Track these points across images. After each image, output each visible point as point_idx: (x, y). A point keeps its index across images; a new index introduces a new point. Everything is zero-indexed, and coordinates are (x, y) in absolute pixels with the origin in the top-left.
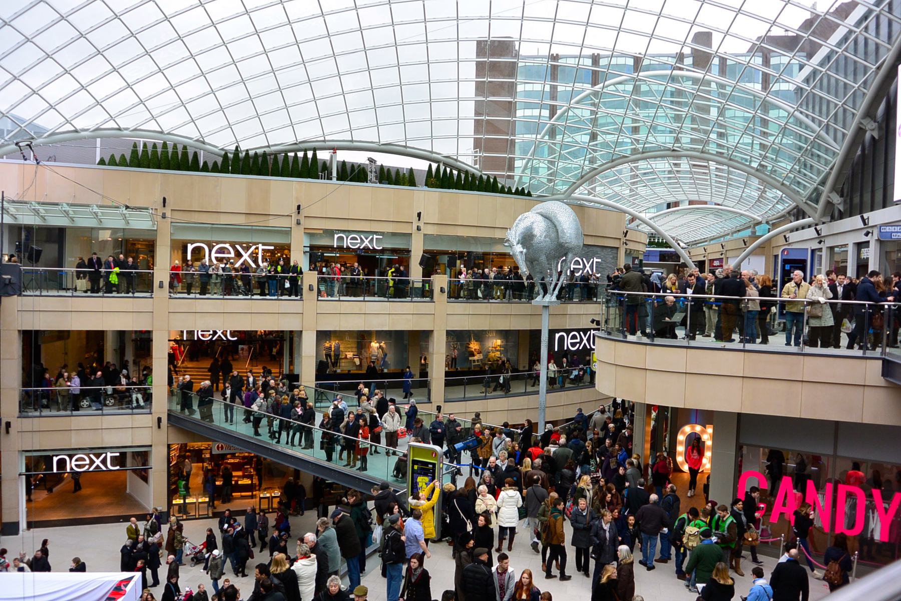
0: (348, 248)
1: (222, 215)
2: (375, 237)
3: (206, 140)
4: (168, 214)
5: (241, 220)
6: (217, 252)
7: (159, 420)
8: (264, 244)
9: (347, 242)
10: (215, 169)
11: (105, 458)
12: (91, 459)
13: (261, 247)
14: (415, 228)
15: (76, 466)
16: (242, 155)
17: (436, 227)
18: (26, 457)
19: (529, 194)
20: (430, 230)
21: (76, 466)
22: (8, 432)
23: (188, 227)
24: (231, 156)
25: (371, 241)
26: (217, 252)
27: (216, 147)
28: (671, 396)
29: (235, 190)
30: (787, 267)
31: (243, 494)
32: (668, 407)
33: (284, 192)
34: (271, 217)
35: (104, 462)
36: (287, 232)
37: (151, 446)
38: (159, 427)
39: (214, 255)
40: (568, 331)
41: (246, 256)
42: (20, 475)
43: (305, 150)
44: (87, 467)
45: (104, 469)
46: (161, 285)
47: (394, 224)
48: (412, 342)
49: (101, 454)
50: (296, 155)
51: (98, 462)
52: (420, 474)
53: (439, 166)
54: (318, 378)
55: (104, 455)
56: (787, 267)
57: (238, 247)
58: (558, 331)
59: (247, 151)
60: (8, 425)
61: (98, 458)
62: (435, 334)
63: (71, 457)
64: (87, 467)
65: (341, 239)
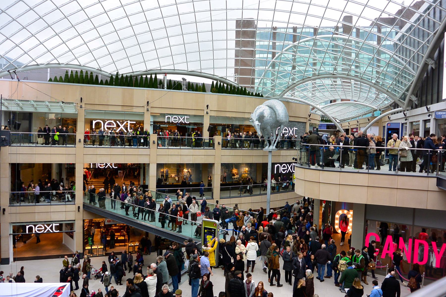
0: (172, 122)
1: (110, 106)
2: (186, 117)
3: (102, 69)
4: (83, 106)
5: (119, 109)
6: (107, 125)
7: (79, 207)
8: (131, 121)
9: (172, 120)
10: (107, 83)
11: (52, 226)
12: (45, 227)
13: (129, 122)
14: (205, 112)
15: (38, 230)
16: (120, 77)
17: (216, 112)
18: (13, 226)
19: (262, 96)
20: (213, 114)
21: (38, 230)
22: (4, 214)
23: (93, 112)
24: (114, 77)
25: (184, 119)
26: (107, 125)
27: (107, 73)
28: (332, 195)
29: (116, 94)
30: (390, 132)
31: (120, 244)
32: (330, 201)
33: (140, 95)
34: (134, 107)
35: (51, 228)
36: (142, 115)
37: (75, 220)
38: (79, 211)
39: (106, 126)
40: (281, 164)
41: (122, 127)
42: (10, 235)
43: (151, 74)
44: (43, 231)
45: (52, 232)
46: (80, 141)
47: (195, 111)
48: (204, 169)
49: (50, 224)
50: (146, 76)
51: (48, 228)
52: (208, 234)
53: (217, 82)
54: (157, 187)
55: (51, 225)
56: (390, 132)
57: (118, 122)
58: (276, 164)
59: (122, 74)
60: (4, 210)
61: (48, 226)
62: (216, 165)
63: (35, 226)
64: (43, 231)
65: (169, 118)
